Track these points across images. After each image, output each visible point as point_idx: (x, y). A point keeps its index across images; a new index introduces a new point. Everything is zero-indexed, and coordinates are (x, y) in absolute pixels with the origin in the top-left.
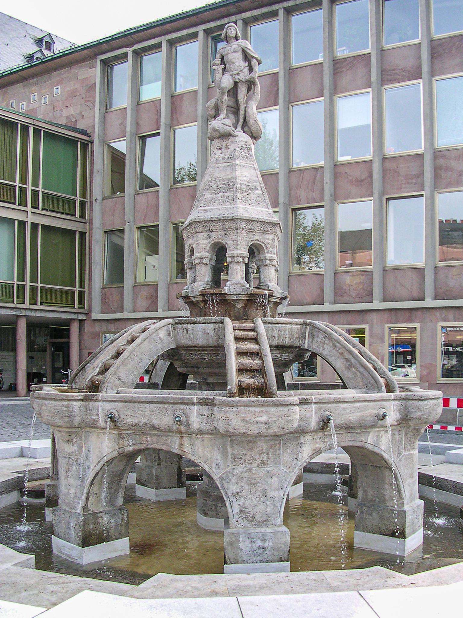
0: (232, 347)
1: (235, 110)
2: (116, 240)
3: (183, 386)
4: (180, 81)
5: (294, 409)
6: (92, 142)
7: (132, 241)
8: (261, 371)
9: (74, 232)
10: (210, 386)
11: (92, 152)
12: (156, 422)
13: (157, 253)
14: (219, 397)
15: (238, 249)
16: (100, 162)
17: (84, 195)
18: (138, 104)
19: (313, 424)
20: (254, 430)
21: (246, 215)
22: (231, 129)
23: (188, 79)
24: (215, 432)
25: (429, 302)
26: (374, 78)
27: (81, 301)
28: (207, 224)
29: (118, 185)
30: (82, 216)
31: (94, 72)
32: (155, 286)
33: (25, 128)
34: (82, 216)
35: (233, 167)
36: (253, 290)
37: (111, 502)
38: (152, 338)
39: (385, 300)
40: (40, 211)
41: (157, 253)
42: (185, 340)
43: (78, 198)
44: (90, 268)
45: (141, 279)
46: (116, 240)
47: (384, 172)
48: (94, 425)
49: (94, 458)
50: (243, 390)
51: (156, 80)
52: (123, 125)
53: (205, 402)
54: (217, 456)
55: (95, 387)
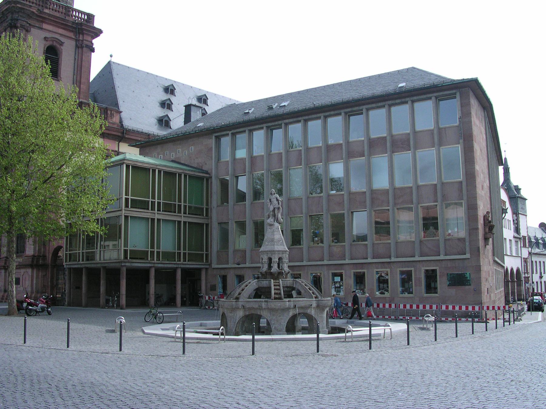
0: (273, 288)
1: (274, 216)
2: (224, 226)
3: (260, 298)
4: (255, 148)
5: (287, 303)
6: (211, 177)
7: (233, 228)
8: (280, 294)
9: (203, 224)
10: (267, 298)
11: (211, 183)
12: (254, 307)
13: (245, 234)
14: (269, 300)
15: (275, 259)
16: (215, 186)
17: (207, 204)
18: (234, 159)
19: (292, 306)
20: (277, 308)
21: (277, 250)
22: (272, 223)
23: (259, 149)
24: (268, 309)
25: (370, 260)
26: (344, 157)
27: (207, 259)
28: (266, 252)
29: (225, 198)
30: (207, 215)
31: (212, 141)
32: (245, 252)
33: (180, 175)
34: (207, 215)
35: (274, 235)
36: (279, 271)
37: (242, 329)
38: (252, 284)
39: (352, 259)
40: (187, 215)
41: (245, 234)
42: (261, 285)
43: (205, 207)
44: (211, 241)
45: (237, 247)
46: (224, 226)
47: (350, 200)
48: (238, 308)
49: (238, 317)
50: (275, 298)
51: (243, 148)
52: (227, 168)
53: (265, 301)
54: (269, 315)
55: (237, 298)
